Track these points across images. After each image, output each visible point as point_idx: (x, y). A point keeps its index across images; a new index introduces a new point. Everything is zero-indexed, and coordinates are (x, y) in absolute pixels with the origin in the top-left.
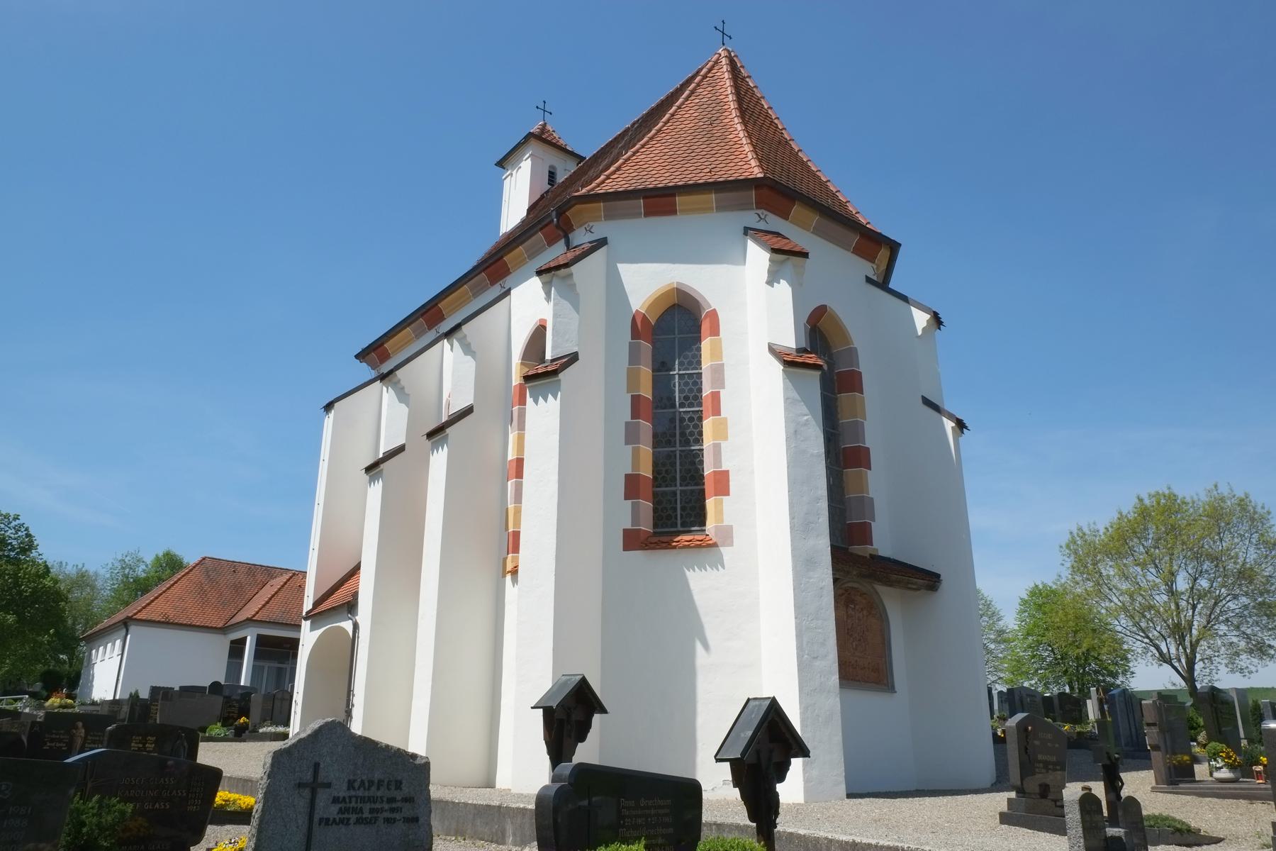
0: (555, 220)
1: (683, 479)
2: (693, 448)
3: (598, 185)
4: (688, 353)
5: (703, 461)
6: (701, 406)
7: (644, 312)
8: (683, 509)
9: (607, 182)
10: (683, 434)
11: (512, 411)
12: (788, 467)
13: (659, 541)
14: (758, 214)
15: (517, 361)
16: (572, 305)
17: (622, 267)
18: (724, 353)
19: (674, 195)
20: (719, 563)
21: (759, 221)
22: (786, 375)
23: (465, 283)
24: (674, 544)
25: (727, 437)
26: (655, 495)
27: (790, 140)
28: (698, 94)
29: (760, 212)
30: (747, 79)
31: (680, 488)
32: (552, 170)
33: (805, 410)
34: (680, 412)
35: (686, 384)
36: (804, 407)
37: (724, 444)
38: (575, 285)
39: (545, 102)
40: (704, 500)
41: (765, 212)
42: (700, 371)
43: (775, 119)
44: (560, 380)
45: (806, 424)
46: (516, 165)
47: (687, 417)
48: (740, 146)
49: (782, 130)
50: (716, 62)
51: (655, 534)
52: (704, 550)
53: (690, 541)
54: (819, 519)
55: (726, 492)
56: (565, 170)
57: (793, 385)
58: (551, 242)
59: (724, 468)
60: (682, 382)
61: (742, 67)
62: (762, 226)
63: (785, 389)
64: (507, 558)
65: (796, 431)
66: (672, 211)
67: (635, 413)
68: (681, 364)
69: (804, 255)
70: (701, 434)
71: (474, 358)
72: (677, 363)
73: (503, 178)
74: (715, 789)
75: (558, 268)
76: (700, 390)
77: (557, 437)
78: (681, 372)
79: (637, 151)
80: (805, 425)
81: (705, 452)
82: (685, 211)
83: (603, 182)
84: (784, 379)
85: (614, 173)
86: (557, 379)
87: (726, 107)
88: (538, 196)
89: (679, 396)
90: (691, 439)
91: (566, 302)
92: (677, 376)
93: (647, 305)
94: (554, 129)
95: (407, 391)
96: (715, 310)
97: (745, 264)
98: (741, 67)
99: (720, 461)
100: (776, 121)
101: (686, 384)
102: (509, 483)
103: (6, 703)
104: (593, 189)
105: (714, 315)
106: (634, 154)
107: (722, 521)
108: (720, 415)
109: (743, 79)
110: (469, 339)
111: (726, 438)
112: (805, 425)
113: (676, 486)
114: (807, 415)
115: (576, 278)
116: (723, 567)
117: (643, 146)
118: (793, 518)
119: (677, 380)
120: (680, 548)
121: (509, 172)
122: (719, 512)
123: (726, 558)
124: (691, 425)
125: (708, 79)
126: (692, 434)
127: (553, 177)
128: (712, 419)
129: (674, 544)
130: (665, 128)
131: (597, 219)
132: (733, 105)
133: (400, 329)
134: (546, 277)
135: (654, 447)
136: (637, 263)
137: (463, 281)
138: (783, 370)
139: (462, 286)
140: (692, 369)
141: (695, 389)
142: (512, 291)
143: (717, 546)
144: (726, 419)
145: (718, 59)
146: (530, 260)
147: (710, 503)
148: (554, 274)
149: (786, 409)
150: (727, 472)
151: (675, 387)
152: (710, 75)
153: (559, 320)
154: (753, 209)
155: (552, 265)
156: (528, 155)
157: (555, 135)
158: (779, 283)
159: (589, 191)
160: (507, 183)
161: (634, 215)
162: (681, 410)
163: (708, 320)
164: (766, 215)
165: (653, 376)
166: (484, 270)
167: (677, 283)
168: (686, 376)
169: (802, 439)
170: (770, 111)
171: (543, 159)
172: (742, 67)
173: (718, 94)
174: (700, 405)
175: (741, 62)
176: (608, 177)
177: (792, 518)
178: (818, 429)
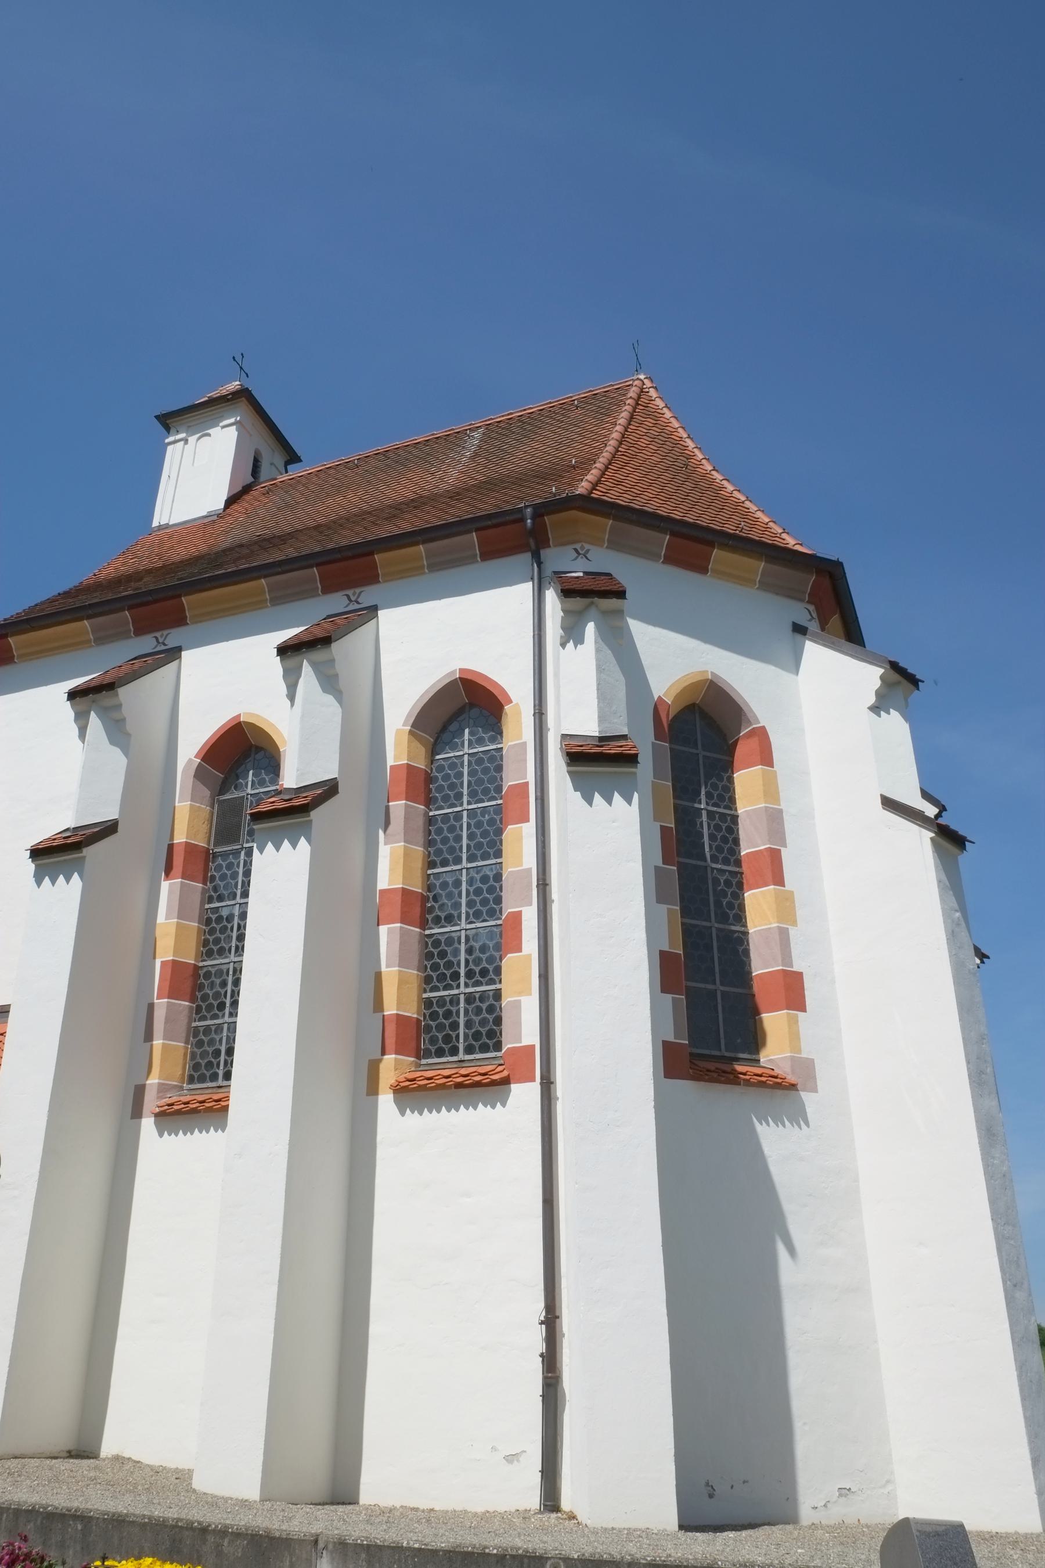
0: (529, 521)
2: (733, 928)
4: (263, 774)
10: (718, 904)
11: (387, 808)
14: (809, 610)
15: (400, 727)
19: (711, 544)
20: (799, 1116)
23: (265, 577)
34: (713, 869)
37: (793, 932)
39: (242, 354)
56: (271, 464)
64: (380, 1060)
66: (700, 567)
67: (775, 856)
68: (709, 796)
72: (703, 792)
74: (829, 1505)
88: (239, 488)
90: (731, 914)
95: (129, 727)
102: (383, 930)
103: (525, 1566)
111: (794, 923)
116: (807, 1124)
121: (182, 435)
123: (810, 1110)
126: (731, 906)
131: (597, 542)
133: (69, 617)
136: (654, 625)
139: (259, 578)
148: (592, 603)
150: (800, 975)
156: (232, 420)
158: (888, 713)
161: (650, 555)
166: (318, 565)
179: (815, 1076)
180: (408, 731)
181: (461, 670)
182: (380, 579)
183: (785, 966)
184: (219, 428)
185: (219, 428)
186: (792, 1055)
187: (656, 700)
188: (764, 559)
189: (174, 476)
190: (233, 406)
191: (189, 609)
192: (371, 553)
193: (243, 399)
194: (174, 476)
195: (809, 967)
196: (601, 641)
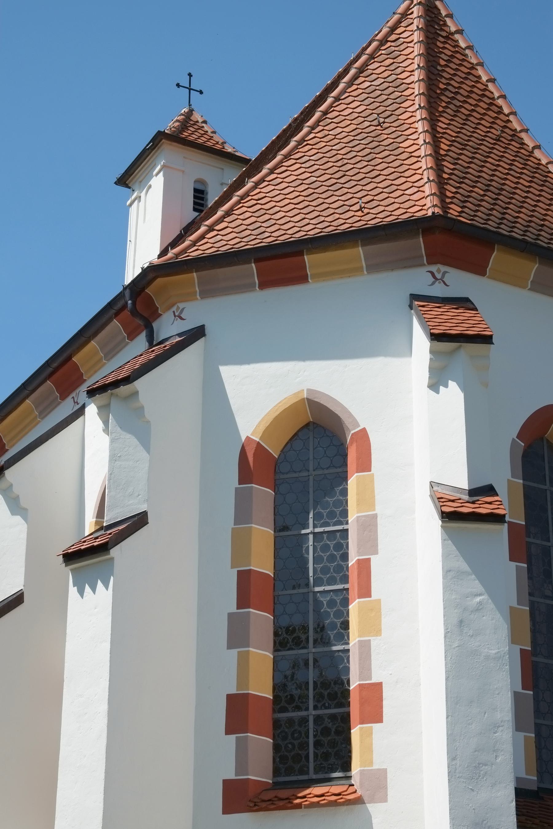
0: (130, 302)
1: (319, 698)
2: (335, 648)
3: (194, 243)
5: (348, 668)
6: (347, 582)
7: (258, 440)
8: (317, 744)
9: (208, 236)
12: (447, 679)
13: (276, 797)
16: (138, 439)
17: (226, 371)
18: (378, 497)
19: (301, 253)
21: (433, 283)
22: (444, 531)
23: (27, 397)
24: (298, 801)
25: (380, 630)
26: (276, 724)
27: (521, 131)
28: (369, 72)
29: (434, 268)
30: (457, 37)
31: (314, 713)
32: (200, 187)
33: (477, 586)
35: (325, 548)
36: (477, 581)
38: (142, 408)
39: (190, 75)
40: (349, 729)
41: (443, 268)
42: (345, 527)
43: (499, 98)
44: (112, 559)
45: (479, 608)
46: (145, 184)
47: (324, 600)
48: (416, 159)
49: (508, 115)
50: (405, 15)
51: (276, 785)
52: (344, 808)
53: (339, 794)
54: (496, 756)
55: (378, 718)
57: (458, 549)
58: (132, 335)
59: (374, 680)
60: (319, 545)
61: (450, 16)
62: (438, 291)
63: (446, 556)
65: (461, 622)
69: (487, 340)
70: (346, 625)
71: (25, 519)
72: (311, 515)
73: (129, 202)
75: (116, 384)
76: (345, 557)
77: (107, 646)
78: (317, 530)
79: (262, 180)
80: (477, 610)
81: (351, 653)
82: (319, 276)
83: (202, 237)
84: (443, 540)
85: (221, 220)
86: (107, 557)
87: (406, 93)
89: (314, 568)
91: (129, 436)
92: (311, 537)
93: (262, 428)
94: (205, 118)
96: (364, 430)
97: (411, 355)
98: (446, 16)
99: (370, 669)
100: (500, 102)
101: (325, 548)
104: (184, 251)
105: (363, 435)
106: (257, 185)
107: (371, 763)
108: (370, 596)
109: (449, 36)
110: (16, 490)
111: (378, 632)
112: (477, 610)
113: (307, 709)
114: (480, 595)
115: (143, 398)
117: (272, 171)
118: (454, 759)
119: (311, 543)
120: (307, 807)
121: (135, 194)
122: (368, 749)
124: (332, 611)
125: (389, 44)
127: (202, 199)
128: (359, 602)
129: (298, 801)
130: (312, 135)
131: (189, 297)
132: (418, 88)
134: (101, 398)
135: (276, 650)
136: (248, 362)
137: (22, 396)
138: (442, 526)
140: (335, 525)
141: (338, 554)
142: (86, 409)
143: (364, 803)
144: (379, 601)
145: (408, 8)
146: (108, 360)
147: (356, 733)
148: (112, 394)
149: (446, 588)
151: (308, 554)
152: (393, 37)
153: (118, 463)
154: (423, 265)
155: (110, 379)
156: (159, 167)
157: (206, 128)
158: (446, 386)
159: (177, 255)
160: (133, 210)
162: (317, 589)
163: (354, 445)
164: (445, 273)
165: (275, 537)
167: (308, 390)
168: (325, 536)
169: (471, 633)
170: (491, 86)
171: (183, 172)
172: (450, 16)
173: (399, 70)
174: (345, 579)
175: (446, 8)
176: (211, 229)
177: (452, 758)
178: (498, 616)
179: (386, 785)
180: (95, 521)
181: (308, 390)
182: (310, 280)
183: (363, 680)
184: (155, 177)
185: (155, 177)
186: (362, 769)
187: (243, 441)
188: (360, 243)
189: (133, 241)
190: (159, 151)
191: (4, 437)
192: (69, 358)
193: (163, 140)
194: (133, 241)
195: (391, 674)
196: (119, 429)
